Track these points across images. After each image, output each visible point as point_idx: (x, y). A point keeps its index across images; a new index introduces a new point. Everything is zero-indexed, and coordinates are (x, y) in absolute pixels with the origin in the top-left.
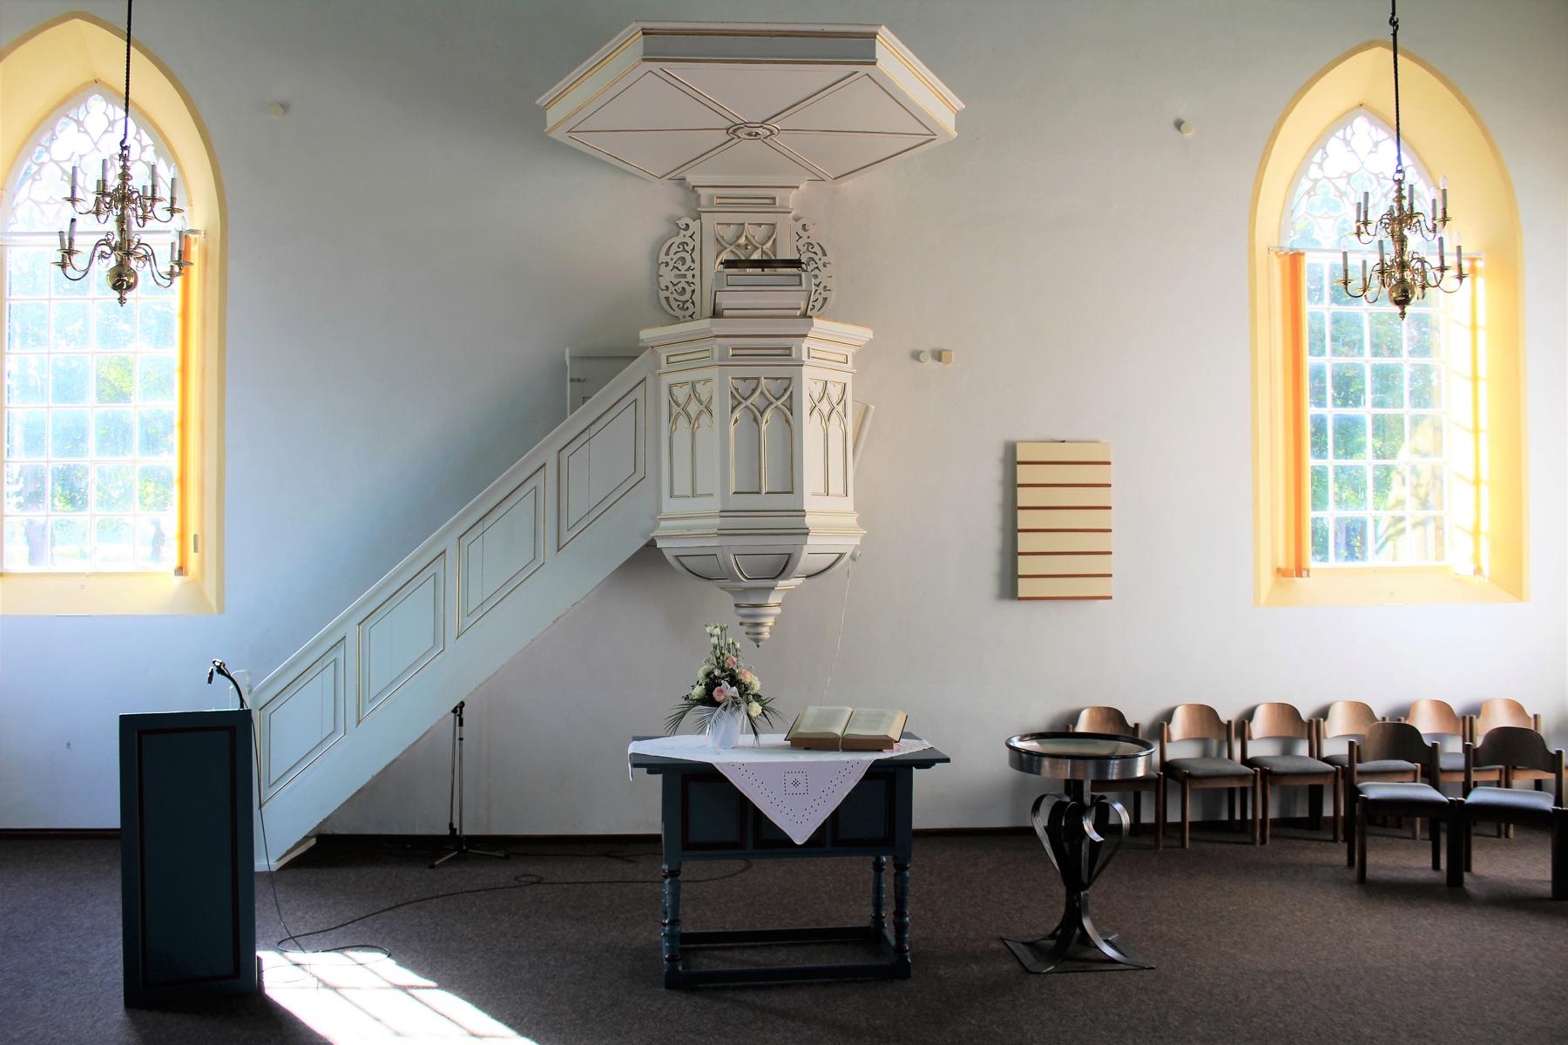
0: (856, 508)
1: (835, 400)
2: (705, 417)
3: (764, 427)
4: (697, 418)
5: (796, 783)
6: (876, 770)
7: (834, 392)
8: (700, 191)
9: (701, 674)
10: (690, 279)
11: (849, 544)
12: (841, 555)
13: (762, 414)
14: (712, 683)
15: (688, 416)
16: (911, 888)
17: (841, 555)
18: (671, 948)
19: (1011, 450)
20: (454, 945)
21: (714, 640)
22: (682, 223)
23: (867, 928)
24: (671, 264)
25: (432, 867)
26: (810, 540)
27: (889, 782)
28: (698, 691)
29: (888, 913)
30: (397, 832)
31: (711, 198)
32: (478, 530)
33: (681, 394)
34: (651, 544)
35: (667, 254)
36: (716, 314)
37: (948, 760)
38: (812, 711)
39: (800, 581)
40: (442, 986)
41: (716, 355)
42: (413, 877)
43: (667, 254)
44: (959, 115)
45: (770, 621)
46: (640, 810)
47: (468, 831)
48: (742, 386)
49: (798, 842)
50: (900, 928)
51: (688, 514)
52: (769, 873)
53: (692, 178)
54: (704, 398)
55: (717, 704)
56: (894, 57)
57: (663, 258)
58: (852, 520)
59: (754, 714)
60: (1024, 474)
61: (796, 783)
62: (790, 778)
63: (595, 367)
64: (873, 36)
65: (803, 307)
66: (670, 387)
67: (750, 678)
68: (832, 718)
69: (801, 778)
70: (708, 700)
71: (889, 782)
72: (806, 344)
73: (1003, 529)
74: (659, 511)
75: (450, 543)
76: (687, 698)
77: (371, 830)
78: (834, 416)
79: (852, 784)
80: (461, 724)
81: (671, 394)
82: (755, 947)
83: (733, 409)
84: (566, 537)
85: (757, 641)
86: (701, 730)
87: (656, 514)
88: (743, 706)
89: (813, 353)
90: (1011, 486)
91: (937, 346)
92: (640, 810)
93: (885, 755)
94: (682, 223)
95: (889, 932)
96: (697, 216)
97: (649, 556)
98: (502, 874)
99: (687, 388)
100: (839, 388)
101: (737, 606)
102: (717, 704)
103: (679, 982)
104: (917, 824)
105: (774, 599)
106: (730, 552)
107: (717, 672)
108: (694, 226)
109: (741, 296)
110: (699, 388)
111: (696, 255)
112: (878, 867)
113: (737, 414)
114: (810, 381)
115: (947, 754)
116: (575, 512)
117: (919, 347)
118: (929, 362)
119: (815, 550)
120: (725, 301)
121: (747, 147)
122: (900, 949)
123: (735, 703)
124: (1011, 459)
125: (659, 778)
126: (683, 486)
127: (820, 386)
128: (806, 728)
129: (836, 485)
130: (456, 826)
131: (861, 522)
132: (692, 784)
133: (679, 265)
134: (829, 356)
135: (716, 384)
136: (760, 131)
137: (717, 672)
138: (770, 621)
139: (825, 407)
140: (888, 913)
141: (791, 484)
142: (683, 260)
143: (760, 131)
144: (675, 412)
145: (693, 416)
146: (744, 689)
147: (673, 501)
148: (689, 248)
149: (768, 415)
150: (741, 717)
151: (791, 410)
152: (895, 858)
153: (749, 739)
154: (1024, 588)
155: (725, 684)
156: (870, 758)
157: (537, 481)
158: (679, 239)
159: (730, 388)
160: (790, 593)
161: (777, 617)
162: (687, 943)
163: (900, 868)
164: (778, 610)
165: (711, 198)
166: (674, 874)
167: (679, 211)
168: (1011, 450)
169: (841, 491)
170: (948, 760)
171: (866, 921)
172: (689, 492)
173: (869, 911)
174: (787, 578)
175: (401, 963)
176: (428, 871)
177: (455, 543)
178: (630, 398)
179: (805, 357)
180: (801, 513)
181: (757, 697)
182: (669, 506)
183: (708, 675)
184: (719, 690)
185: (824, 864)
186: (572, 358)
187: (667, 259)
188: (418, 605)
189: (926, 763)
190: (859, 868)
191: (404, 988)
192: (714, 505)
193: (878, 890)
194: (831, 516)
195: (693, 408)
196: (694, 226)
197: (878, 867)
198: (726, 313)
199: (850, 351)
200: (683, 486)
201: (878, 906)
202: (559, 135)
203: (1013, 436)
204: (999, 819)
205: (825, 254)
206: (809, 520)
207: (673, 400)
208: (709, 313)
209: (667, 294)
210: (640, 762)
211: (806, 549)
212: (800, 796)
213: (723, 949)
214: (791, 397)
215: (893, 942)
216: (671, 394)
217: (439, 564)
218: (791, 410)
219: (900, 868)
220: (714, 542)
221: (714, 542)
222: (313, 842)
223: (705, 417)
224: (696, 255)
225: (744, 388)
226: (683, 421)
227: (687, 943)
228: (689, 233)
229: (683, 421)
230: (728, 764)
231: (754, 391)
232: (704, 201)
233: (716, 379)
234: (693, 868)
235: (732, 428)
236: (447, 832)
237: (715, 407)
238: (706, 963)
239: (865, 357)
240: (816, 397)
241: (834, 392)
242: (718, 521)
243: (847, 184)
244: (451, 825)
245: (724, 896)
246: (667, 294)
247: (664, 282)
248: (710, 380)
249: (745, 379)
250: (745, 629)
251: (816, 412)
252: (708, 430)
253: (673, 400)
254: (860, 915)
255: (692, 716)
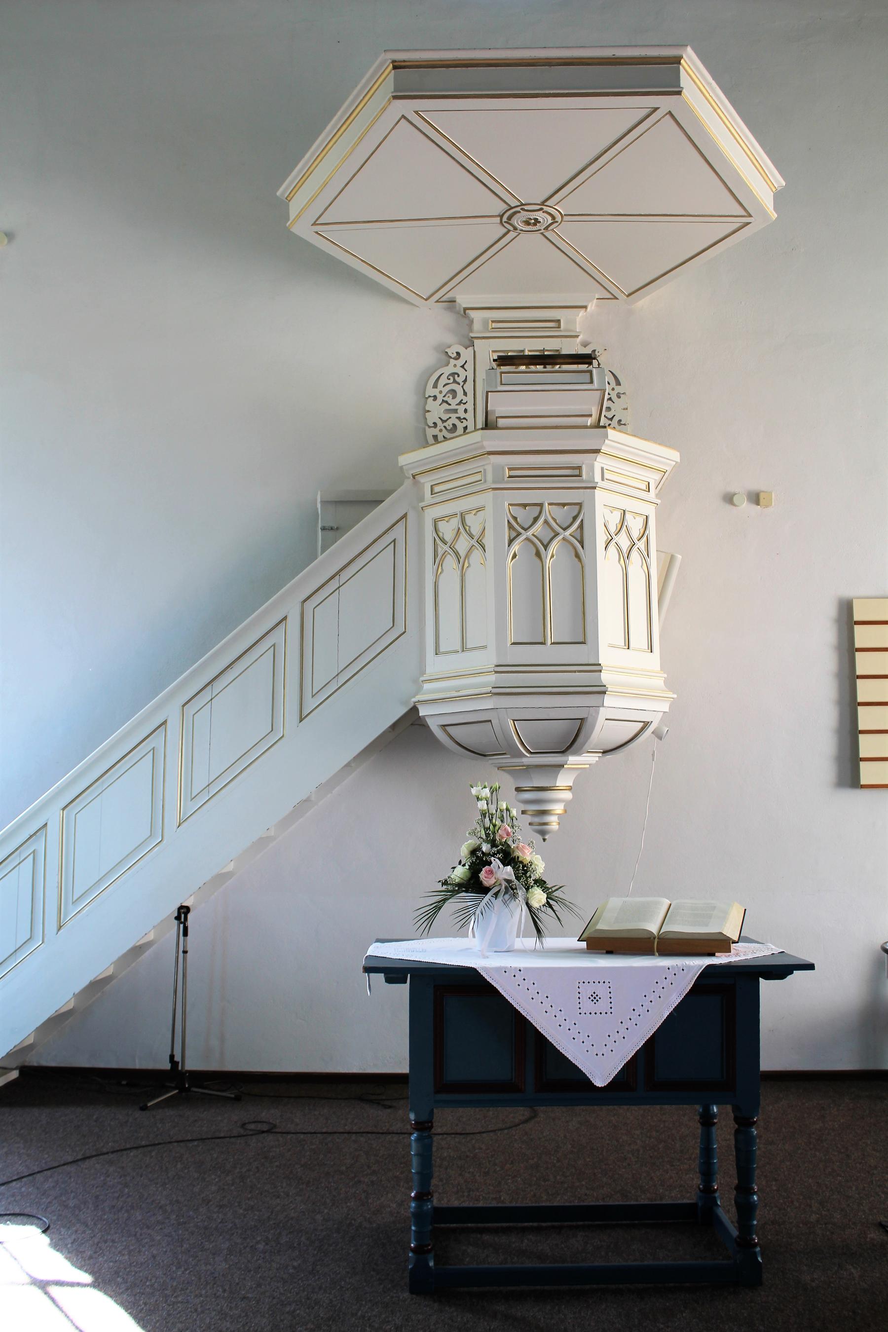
0: (662, 668)
1: (635, 535)
2: (477, 554)
3: (548, 562)
4: (467, 556)
5: (594, 998)
6: (712, 984)
7: (635, 525)
8: (472, 314)
9: (464, 851)
10: (461, 414)
11: (655, 710)
12: (646, 725)
13: (546, 547)
14: (478, 861)
15: (457, 554)
16: (759, 1149)
17: (646, 725)
18: (419, 1235)
19: (846, 608)
20: (138, 1215)
21: (482, 805)
22: (452, 352)
23: (693, 1206)
24: (440, 398)
25: (144, 1108)
26: (608, 700)
27: (726, 996)
28: (460, 873)
29: (724, 1184)
30: (114, 1065)
31: (485, 322)
32: (206, 696)
33: (448, 530)
34: (414, 710)
35: (435, 386)
36: (488, 425)
37: (811, 967)
38: (615, 902)
39: (593, 758)
40: (101, 1282)
41: (490, 477)
42: (114, 1121)
43: (435, 386)
44: (779, 197)
45: (558, 808)
46: (379, 1038)
47: (192, 1064)
48: (519, 512)
49: (599, 1083)
50: (745, 1210)
51: (457, 668)
52: (559, 1123)
53: (464, 300)
54: (476, 531)
55: (485, 890)
56: (700, 90)
57: (430, 391)
58: (659, 682)
59: (535, 904)
60: (863, 636)
61: (594, 998)
62: (587, 991)
63: (351, 506)
64: (677, 60)
65: (595, 412)
66: (435, 522)
67: (527, 855)
68: (645, 911)
69: (601, 990)
70: (474, 885)
71: (726, 996)
72: (600, 462)
73: (840, 703)
74: (423, 673)
75: (172, 713)
76: (445, 883)
77: (83, 1062)
78: (635, 554)
79: (675, 1000)
80: (185, 933)
81: (436, 530)
82: (539, 1229)
83: (511, 542)
84: (310, 703)
85: (543, 833)
86: (461, 928)
87: (419, 677)
88: (521, 892)
89: (606, 476)
90: (848, 651)
91: (754, 486)
92: (379, 1038)
93: (720, 959)
94: (452, 352)
95: (726, 1213)
96: (470, 343)
97: (409, 735)
98: (225, 1119)
99: (455, 522)
100: (640, 521)
101: (518, 789)
102: (485, 890)
103: (433, 1284)
104: (767, 1063)
105: (564, 780)
106: (509, 718)
107: (485, 848)
108: (467, 354)
109: (517, 400)
110: (469, 519)
111: (469, 387)
112: (707, 1120)
113: (516, 547)
114: (605, 508)
115: (811, 960)
116: (323, 670)
117: (731, 489)
118: (745, 506)
119: (611, 719)
120: (500, 405)
121: (529, 244)
122: (745, 1243)
123: (510, 889)
124: (847, 619)
125: (404, 989)
126: (450, 638)
127: (617, 516)
128: (607, 925)
129: (639, 636)
130: (178, 1058)
131: (670, 684)
132: (450, 999)
133: (449, 399)
134: (626, 477)
135: (490, 513)
136: (540, 216)
137: (485, 848)
138: (558, 808)
139: (623, 541)
140: (724, 1184)
141: (583, 633)
142: (454, 393)
143: (540, 216)
144: (440, 552)
145: (462, 554)
146: (523, 870)
147: (440, 658)
148: (460, 380)
149: (554, 547)
150: (518, 913)
151: (582, 543)
152: (736, 1109)
153: (531, 942)
154: (868, 773)
155: (496, 862)
156: (702, 962)
157: (277, 637)
158: (450, 369)
159: (507, 517)
160: (583, 774)
161: (568, 804)
162: (443, 1225)
163: (744, 1123)
164: (568, 795)
165: (498, 469)
166: (424, 1127)
167: (449, 338)
168: (846, 608)
169: (645, 645)
170: (811, 967)
171: (690, 1198)
172: (459, 648)
173: (697, 1181)
174: (577, 753)
175: (56, 1245)
176: (138, 1114)
177: (178, 709)
178: (388, 538)
179: (598, 478)
180: (596, 668)
181: (540, 883)
182: (434, 665)
183: (473, 852)
184: (487, 872)
185: (631, 1114)
186: (323, 502)
187: (435, 392)
188: (134, 782)
189: (779, 971)
190: (679, 1120)
191: (43, 1285)
192: (488, 659)
193: (707, 1152)
194: (633, 676)
195: (463, 545)
196: (467, 354)
197: (707, 1120)
198: (501, 422)
199: (653, 478)
200: (450, 638)
201: (707, 1173)
202: (302, 229)
203: (847, 592)
204: (844, 1061)
205: (618, 383)
206: (606, 677)
207: (439, 538)
208: (480, 423)
209: (435, 431)
210: (394, 973)
211: (603, 713)
212: (600, 1020)
213: (496, 1231)
214: (581, 526)
215: (735, 1232)
216: (436, 530)
217: (159, 737)
218: (582, 543)
219: (744, 1123)
220: (488, 704)
221: (488, 704)
222: (14, 1075)
223: (477, 554)
224: (469, 387)
225: (525, 517)
226: (450, 562)
227: (443, 1225)
228: (460, 362)
229: (450, 562)
230: (498, 969)
231: (536, 519)
232: (477, 326)
233: (489, 509)
234: (447, 1118)
235: (510, 563)
236: (167, 1066)
237: (488, 541)
238: (476, 1254)
239: (672, 489)
240: (613, 530)
241: (635, 525)
242: (492, 678)
243: (644, 302)
244: (172, 1057)
245: (494, 1156)
246: (435, 431)
247: (431, 418)
248: (479, 509)
249: (525, 506)
250: (528, 818)
251: (612, 548)
252: (481, 570)
253: (439, 538)
254: (679, 1187)
255: (452, 906)
